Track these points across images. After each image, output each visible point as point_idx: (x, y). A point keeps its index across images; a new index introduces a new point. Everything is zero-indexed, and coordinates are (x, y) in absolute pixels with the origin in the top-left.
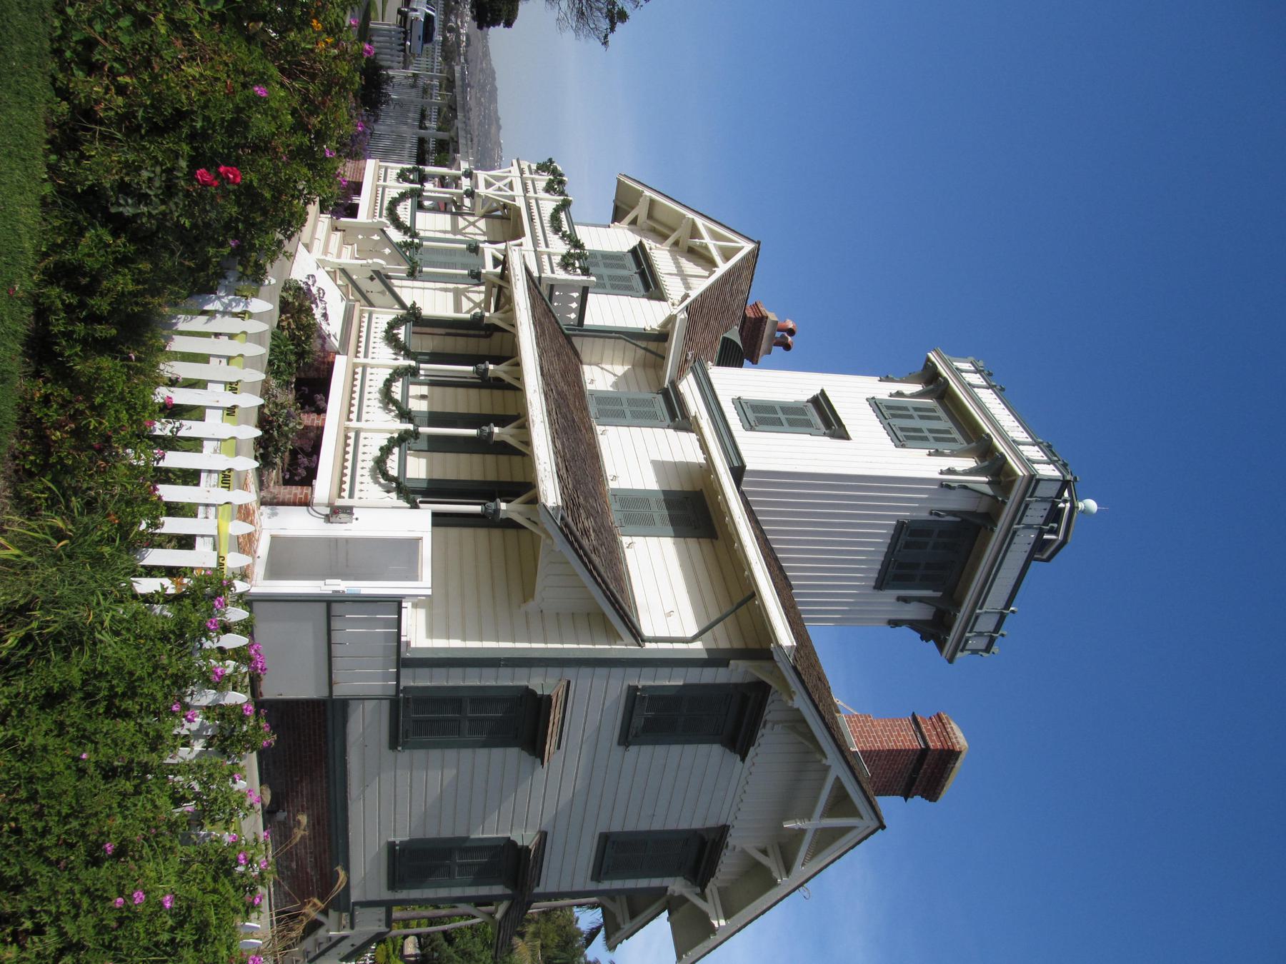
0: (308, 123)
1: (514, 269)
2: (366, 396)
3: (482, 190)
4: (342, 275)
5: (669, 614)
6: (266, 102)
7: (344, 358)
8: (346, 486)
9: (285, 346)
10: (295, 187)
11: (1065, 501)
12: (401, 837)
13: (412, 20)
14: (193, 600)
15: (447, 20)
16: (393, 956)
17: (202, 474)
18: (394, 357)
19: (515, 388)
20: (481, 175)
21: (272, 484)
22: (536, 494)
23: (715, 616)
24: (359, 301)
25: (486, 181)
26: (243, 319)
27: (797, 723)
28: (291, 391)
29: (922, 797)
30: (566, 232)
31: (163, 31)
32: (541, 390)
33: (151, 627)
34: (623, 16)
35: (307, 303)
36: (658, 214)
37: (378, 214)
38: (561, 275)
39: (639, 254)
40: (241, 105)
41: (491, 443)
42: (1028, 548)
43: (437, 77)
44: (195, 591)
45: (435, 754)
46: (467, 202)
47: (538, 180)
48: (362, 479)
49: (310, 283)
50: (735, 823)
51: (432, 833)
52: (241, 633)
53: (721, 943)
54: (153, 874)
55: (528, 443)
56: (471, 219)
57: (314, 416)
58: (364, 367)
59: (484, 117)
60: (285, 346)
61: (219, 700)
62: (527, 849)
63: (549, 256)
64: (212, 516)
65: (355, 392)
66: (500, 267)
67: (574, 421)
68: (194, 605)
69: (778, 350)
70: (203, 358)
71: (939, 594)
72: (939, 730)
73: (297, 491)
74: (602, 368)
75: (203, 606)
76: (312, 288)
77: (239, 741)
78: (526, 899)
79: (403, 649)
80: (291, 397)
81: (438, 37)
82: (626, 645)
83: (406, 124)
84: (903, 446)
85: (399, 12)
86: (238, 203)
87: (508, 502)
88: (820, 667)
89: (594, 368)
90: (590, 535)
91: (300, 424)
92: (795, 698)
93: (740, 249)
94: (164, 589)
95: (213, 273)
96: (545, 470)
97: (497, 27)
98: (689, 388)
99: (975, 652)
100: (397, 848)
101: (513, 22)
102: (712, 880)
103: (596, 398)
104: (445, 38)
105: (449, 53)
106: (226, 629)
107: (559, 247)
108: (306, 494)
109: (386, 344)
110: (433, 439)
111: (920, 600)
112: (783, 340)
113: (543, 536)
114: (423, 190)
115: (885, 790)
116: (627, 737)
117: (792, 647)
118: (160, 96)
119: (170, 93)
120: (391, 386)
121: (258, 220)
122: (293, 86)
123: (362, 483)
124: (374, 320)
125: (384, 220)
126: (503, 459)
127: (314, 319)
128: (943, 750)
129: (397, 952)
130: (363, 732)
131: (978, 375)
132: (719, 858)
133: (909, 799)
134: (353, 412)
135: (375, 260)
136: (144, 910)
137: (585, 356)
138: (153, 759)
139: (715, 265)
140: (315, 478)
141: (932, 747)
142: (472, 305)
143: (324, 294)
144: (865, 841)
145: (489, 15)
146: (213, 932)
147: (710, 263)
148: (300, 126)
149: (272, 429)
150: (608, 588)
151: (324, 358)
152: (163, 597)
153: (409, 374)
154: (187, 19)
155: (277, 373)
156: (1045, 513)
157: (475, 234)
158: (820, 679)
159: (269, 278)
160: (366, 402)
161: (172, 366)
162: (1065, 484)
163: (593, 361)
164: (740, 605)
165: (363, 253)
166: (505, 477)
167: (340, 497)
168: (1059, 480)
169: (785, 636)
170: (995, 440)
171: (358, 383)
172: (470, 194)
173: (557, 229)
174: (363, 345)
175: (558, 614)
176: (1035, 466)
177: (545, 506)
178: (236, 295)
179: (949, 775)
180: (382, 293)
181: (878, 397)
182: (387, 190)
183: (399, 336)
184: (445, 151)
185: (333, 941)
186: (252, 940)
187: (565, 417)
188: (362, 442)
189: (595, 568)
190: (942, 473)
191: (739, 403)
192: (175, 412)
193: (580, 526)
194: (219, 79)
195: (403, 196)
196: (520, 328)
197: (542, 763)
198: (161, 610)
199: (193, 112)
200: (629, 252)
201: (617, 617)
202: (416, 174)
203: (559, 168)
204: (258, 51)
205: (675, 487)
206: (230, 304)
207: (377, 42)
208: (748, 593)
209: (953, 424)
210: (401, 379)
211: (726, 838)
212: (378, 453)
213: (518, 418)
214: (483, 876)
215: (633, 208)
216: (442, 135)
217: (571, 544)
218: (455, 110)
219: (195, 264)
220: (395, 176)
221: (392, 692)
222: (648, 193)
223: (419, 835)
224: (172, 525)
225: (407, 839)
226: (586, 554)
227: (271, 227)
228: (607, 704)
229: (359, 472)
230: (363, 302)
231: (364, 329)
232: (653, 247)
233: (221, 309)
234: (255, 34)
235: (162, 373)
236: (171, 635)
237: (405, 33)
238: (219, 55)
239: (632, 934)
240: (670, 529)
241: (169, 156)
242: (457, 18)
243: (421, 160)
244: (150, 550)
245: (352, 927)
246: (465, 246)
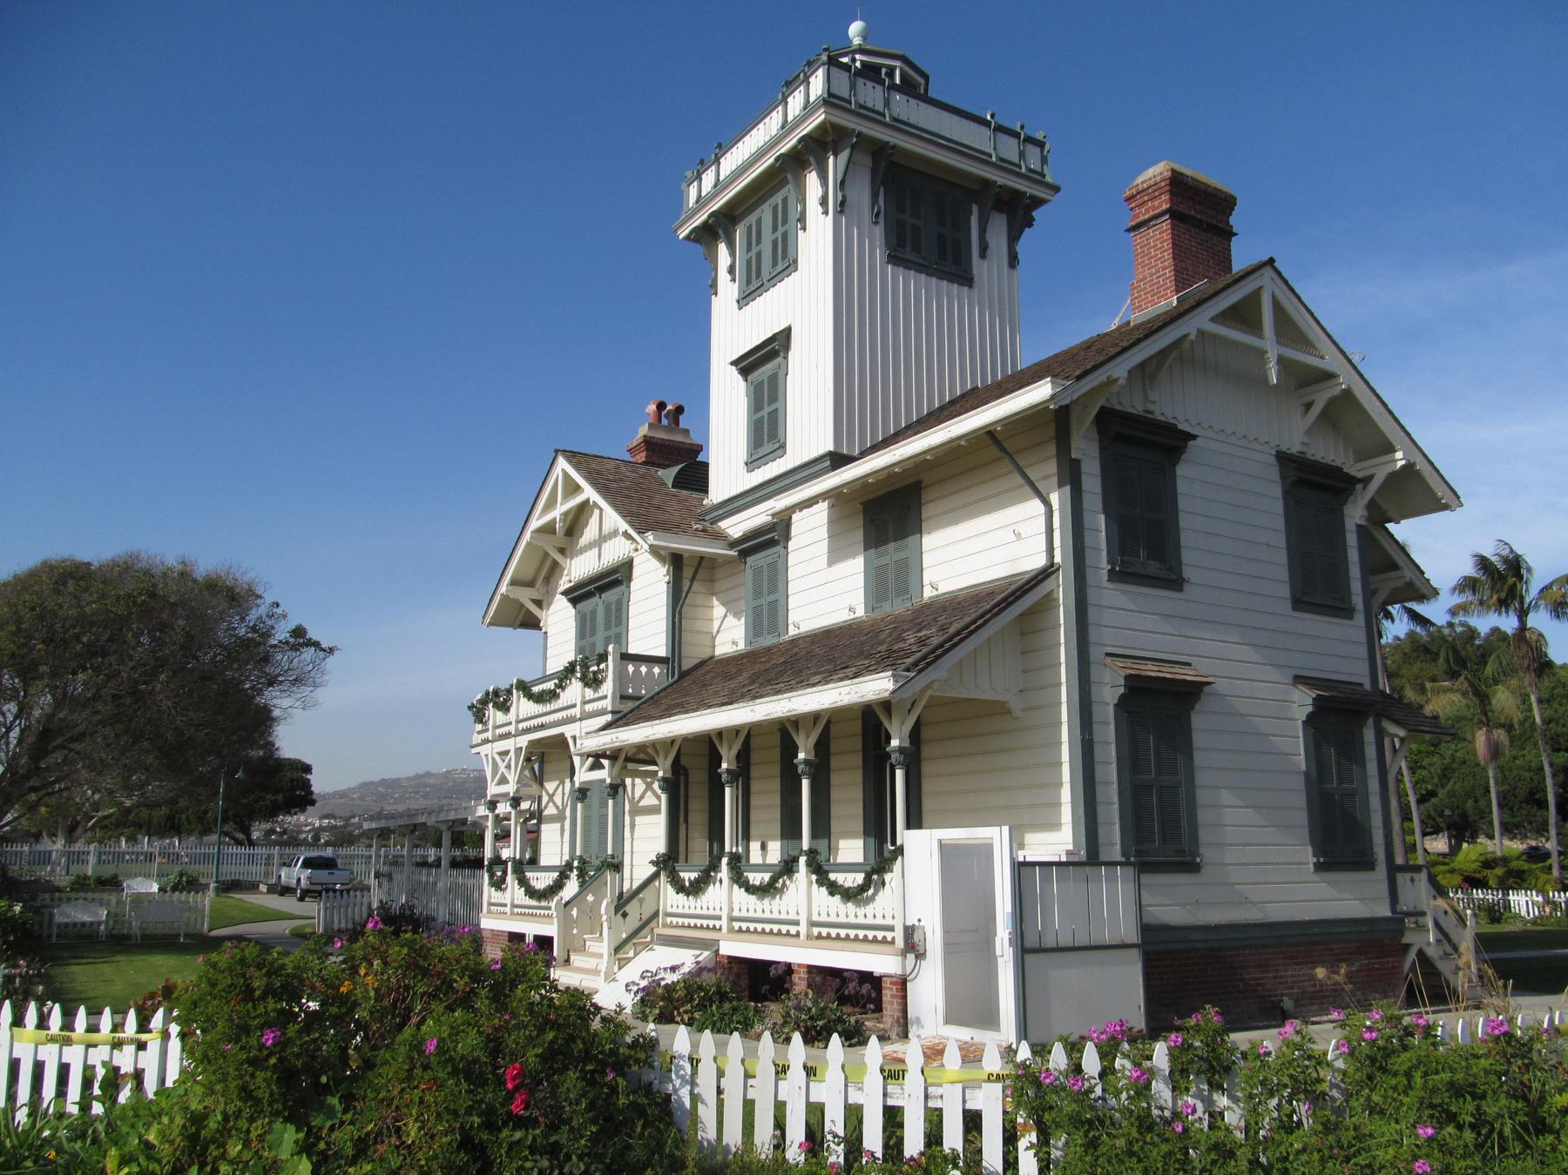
0: (464, 992)
1: (604, 744)
2: (767, 915)
3: (510, 788)
4: (622, 951)
5: (1018, 536)
6: (444, 1039)
7: (722, 943)
8: (880, 935)
9: (714, 1015)
10: (538, 1004)
11: (854, 60)
12: (1308, 856)
13: (311, 883)
14: (1044, 1110)
15: (305, 843)
16: (1452, 865)
17: (889, 1104)
18: (718, 884)
19: (748, 736)
20: (493, 789)
21: (881, 1026)
22: (878, 703)
24: (652, 929)
25: (499, 783)
26: (698, 1061)
27: (1146, 373)
28: (765, 1007)
29: (1231, 214)
30: (555, 684)
31: (369, 1167)
32: (751, 703)
33: (1081, 1160)
34: (299, 632)
35: (660, 991)
36: (528, 574)
37: (546, 912)
38: (608, 688)
39: (577, 595)
40: (450, 1069)
41: (818, 761)
42: (913, 102)
43: (378, 850)
44: (1033, 1108)
45: (1203, 816)
46: (525, 805)
47: (495, 722)
48: (870, 916)
49: (635, 988)
50: (1273, 444)
51: (1302, 818)
52: (1081, 1051)
53: (1425, 456)
54: (1391, 1151)
55: (815, 716)
56: (545, 799)
57: (795, 978)
58: (732, 919)
59: (418, 792)
60: (714, 1015)
61: (1164, 1076)
62: (1317, 700)
63: (585, 703)
64: (939, 1091)
65: (763, 929)
66: (603, 761)
67: (785, 662)
68: (1051, 1108)
69: (684, 421)
70: (749, 1107)
71: (975, 209)
72: (1146, 198)
73: (889, 995)
74: (718, 632)
75: (1053, 1098)
76: (641, 986)
77: (1214, 1050)
78: (1379, 699)
79: (1075, 859)
80: (772, 1006)
81: (329, 852)
82: (1059, 586)
83: (435, 884)
84: (795, 261)
85: (302, 899)
86: (565, 1069)
87: (888, 738)
88: (1073, 348)
90: (925, 635)
91: (806, 994)
92: (1115, 376)
93: (565, 474)
94: (1032, 1146)
95: (647, 1098)
96: (849, 693)
97: (312, 782)
98: (736, 526)
99: (1044, 160)
100: (1321, 860)
101: (305, 764)
102: (1345, 470)
104: (327, 844)
105: (344, 838)
106: (1077, 1069)
107: (575, 691)
108: (892, 983)
109: (703, 894)
110: (815, 834)
111: (983, 231)
112: (671, 416)
113: (929, 693)
114: (514, 858)
115: (1225, 261)
116: (1173, 581)
117: (1052, 382)
118: (446, 1168)
119: (441, 1156)
120: (754, 886)
121: (581, 1046)
122: (420, 1012)
123: (884, 917)
124: (674, 910)
125: (553, 904)
126: (835, 746)
127: (678, 981)
128: (1171, 192)
129: (1447, 861)
130: (1180, 905)
131: (704, 176)
132: (1317, 462)
133: (1234, 230)
134: (788, 931)
135: (603, 911)
136: (1438, 1160)
137: (704, 654)
138: (1243, 1155)
139: (587, 501)
140: (872, 973)
141: (1168, 206)
142: (649, 793)
143: (647, 971)
144: (1290, 282)
145: (298, 793)
146: (1460, 1076)
147: (584, 509)
148: (466, 1001)
149: (815, 1027)
150: (990, 610)
151: (724, 968)
152: (1041, 1148)
153: (738, 865)
154: (352, 1140)
155: (747, 1025)
156: (870, 84)
157: (564, 794)
158: (1089, 347)
159: (648, 1031)
160: (775, 916)
161: (763, 1144)
162: (833, 62)
164: (1003, 449)
165: (595, 928)
166: (858, 743)
167: (893, 942)
168: (828, 70)
169: (1041, 392)
170: (782, 151)
171: (752, 926)
172: (516, 802)
173: (552, 695)
174: (705, 922)
175: (1024, 672)
176: (812, 100)
177: (894, 692)
178: (670, 1071)
179: (1202, 183)
180: (641, 901)
181: (736, 295)
182: (516, 902)
183: (692, 879)
184: (465, 836)
185: (1441, 937)
186: (1459, 1032)
187: (781, 674)
188: (823, 918)
189: (966, 627)
190: (826, 213)
191: (752, 464)
192: (815, 1139)
193: (914, 648)
194: (421, 1098)
195: (523, 882)
196: (676, 734)
197: (1209, 683)
198: (1057, 1149)
199: (462, 1127)
200: (575, 607)
201: (1024, 598)
202: (495, 868)
203: (479, 697)
204: (384, 1054)
205: (859, 535)
206: (682, 1077)
207: (340, 923)
208: (989, 441)
209: (763, 203)
210: (745, 874)
211: (1292, 455)
212: (838, 897)
213: (785, 730)
214: (1352, 752)
215: (522, 606)
216: (446, 841)
217: (938, 658)
218: (415, 826)
219: (639, 1119)
220: (499, 894)
221: (1130, 870)
222: (503, 589)
223: (1305, 833)
224: (953, 1138)
225: (1310, 849)
226: (950, 639)
227: (588, 1030)
228: (1132, 607)
229: (861, 920)
230: (653, 924)
231: (687, 921)
232: (567, 578)
233: (688, 1087)
234: (364, 1060)
235: (770, 1157)
236: (1091, 1135)
237: (327, 891)
238: (392, 1099)
239: (1418, 567)
240: (911, 540)
241: (516, 1152)
242: (302, 832)
243: (477, 863)
244: (984, 1164)
245: (1423, 914)
246: (579, 805)
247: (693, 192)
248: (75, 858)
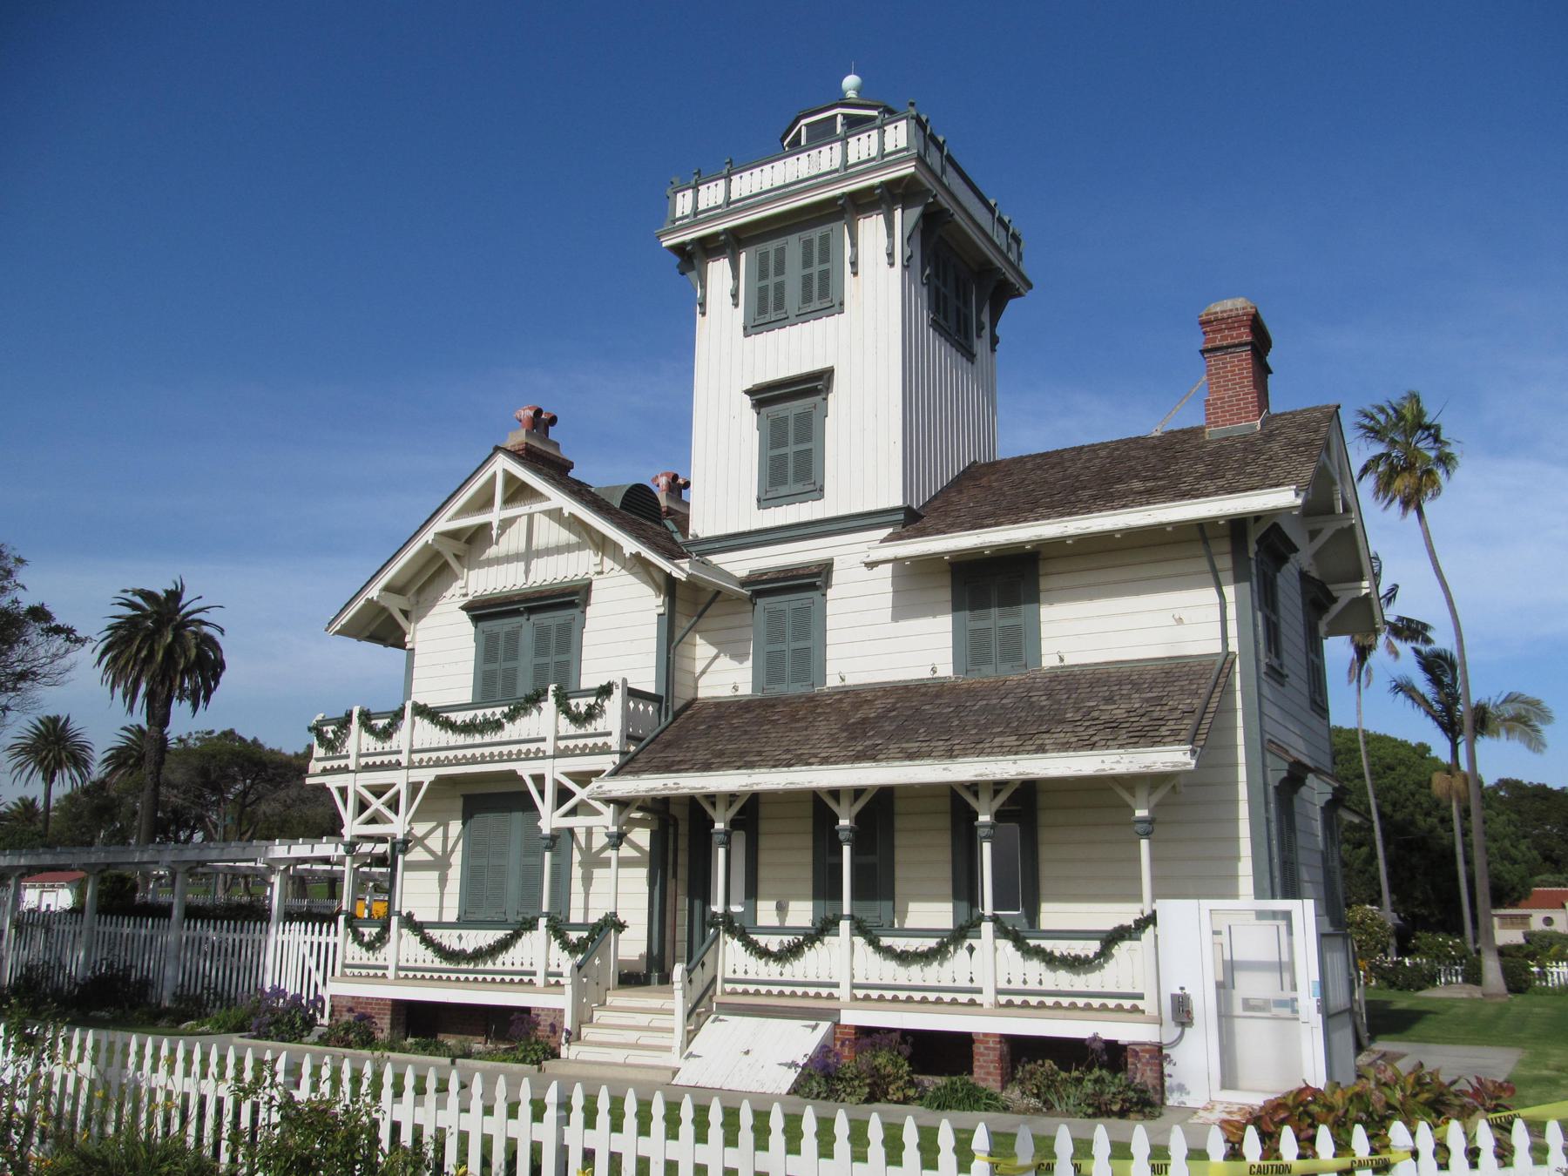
5: (1180, 621)
23: (1204, 565)
72: (1224, 326)
74: (703, 673)
89: (701, 683)
103: (769, 682)
163: (693, 685)
205: (946, 595)
222: (374, 592)
240: (1025, 609)
247: (683, 203)
248: (57, 918)
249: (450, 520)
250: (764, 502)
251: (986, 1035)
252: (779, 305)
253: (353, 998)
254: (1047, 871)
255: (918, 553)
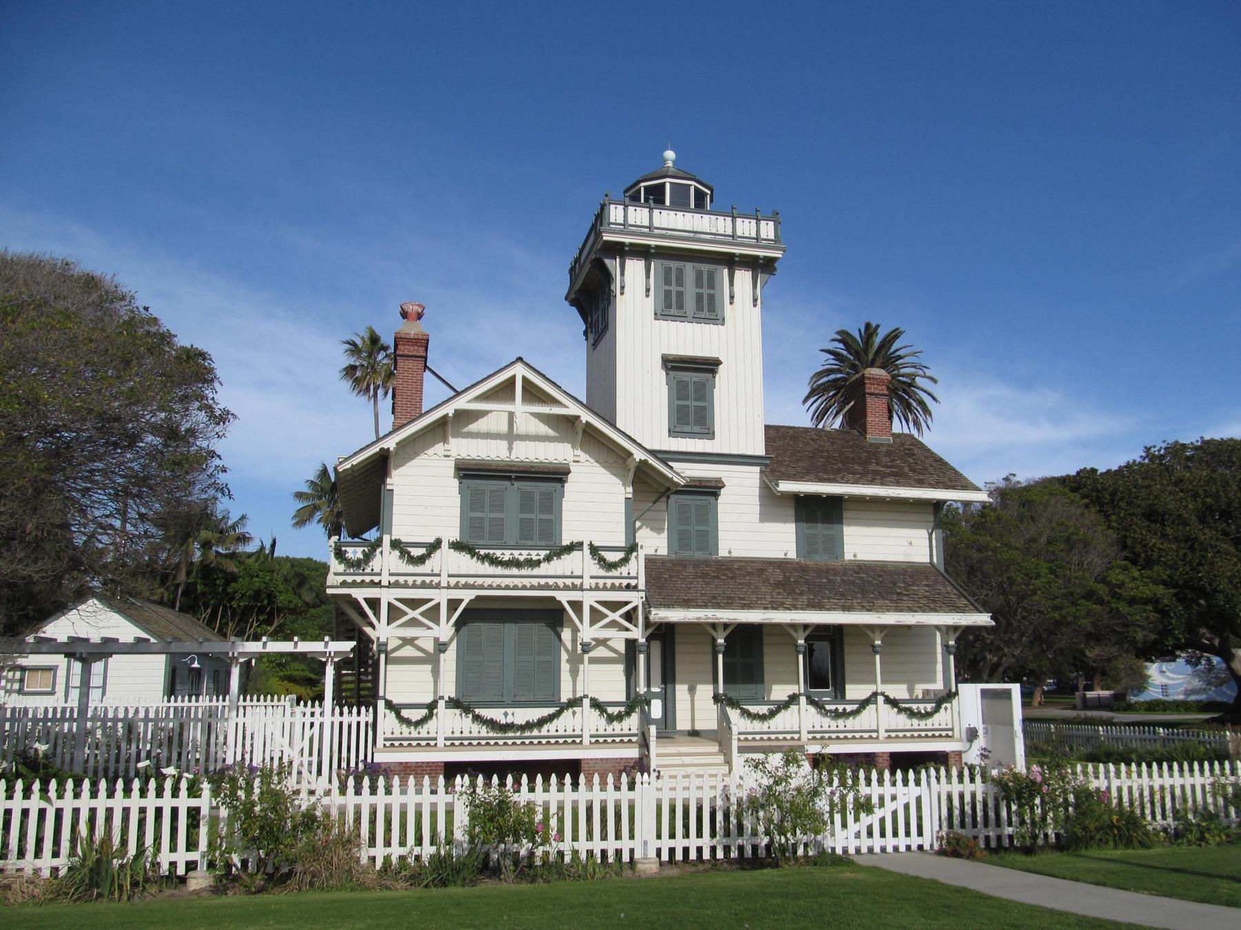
205: (792, 512)
249: (469, 401)
250: (672, 433)
251: (883, 753)
252: (680, 306)
253: (401, 763)
254: (848, 667)
255: (787, 490)
